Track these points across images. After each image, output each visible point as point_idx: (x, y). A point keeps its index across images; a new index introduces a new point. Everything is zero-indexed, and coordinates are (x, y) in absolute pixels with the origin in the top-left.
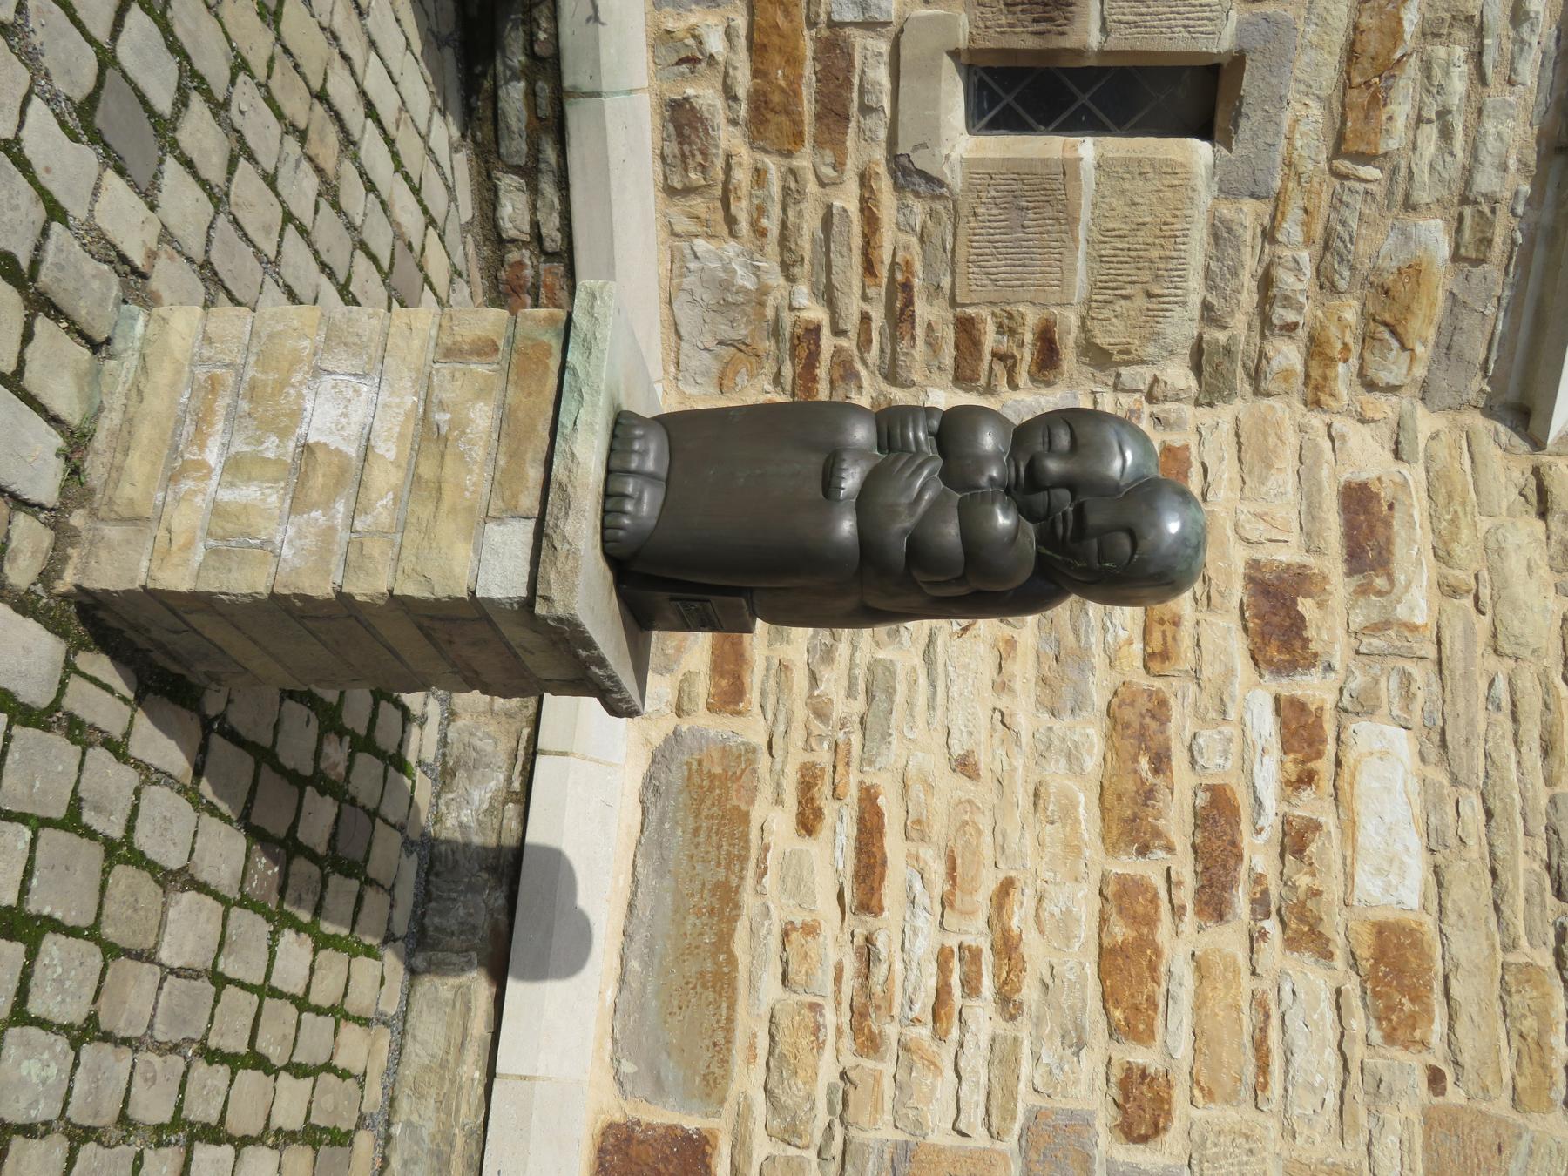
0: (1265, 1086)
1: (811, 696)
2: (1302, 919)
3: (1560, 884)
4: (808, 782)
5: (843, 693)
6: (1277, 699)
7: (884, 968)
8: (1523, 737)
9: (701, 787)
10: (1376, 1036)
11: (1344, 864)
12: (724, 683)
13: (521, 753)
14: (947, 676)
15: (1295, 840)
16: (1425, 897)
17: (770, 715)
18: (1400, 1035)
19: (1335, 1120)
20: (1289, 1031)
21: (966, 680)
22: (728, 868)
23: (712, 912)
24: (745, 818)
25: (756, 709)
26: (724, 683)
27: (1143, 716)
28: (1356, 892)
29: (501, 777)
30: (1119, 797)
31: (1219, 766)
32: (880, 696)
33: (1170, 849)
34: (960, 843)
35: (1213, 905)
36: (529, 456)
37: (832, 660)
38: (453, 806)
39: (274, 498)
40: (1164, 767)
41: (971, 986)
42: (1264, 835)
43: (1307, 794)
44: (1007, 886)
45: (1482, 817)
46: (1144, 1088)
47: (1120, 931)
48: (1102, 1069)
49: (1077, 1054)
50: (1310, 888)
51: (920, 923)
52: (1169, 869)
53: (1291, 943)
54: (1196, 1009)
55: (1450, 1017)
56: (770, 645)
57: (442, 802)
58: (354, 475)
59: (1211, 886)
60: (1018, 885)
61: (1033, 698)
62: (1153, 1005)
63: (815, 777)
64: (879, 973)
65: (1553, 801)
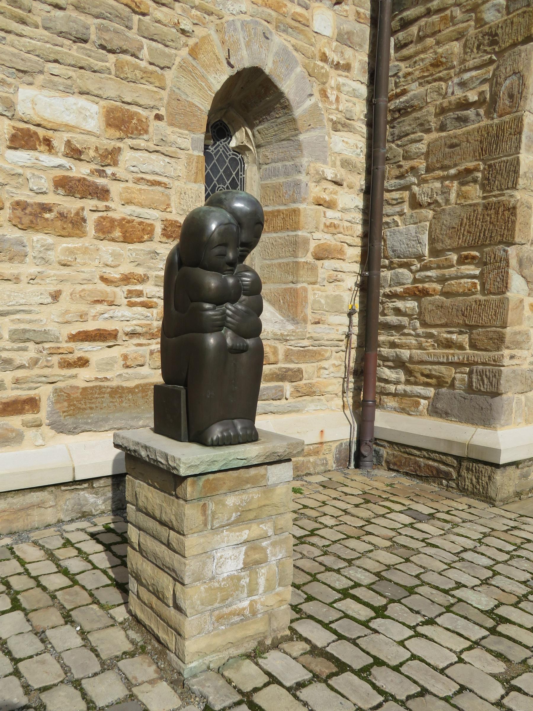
1: (28, 368)
2: (107, 157)
3: (83, 40)
4: (67, 365)
5: (26, 353)
6: (10, 148)
7: (137, 328)
8: (19, 31)
9: (74, 410)
10: (145, 137)
11: (83, 134)
12: (27, 407)
13: (72, 487)
14: (14, 305)
15: (75, 153)
16: (93, 102)
17: (39, 385)
18: (145, 127)
20: (147, 171)
21: (15, 296)
22: (104, 393)
23: (120, 397)
24: (85, 389)
25: (36, 391)
26: (27, 407)
27: (26, 214)
28: (95, 131)
29: (82, 493)
30: (64, 228)
31: (45, 183)
32: (27, 336)
33: (83, 209)
34: (88, 298)
35: (102, 193)
36: (247, 476)
37: (11, 359)
38: (97, 508)
39: (263, 571)
40: (48, 207)
41: (140, 294)
43: (55, 143)
44: (103, 279)
45: (57, 65)
46: (168, 229)
47: (117, 233)
48: (163, 245)
49: (158, 254)
51: (120, 314)
52: (91, 210)
53: (115, 164)
54: (142, 206)
55: (136, 105)
56: (5, 389)
57: (96, 513)
58: (252, 544)
60: (102, 274)
61: (19, 265)
62: (140, 223)
63: (65, 362)
64: (139, 330)
65: (46, 28)
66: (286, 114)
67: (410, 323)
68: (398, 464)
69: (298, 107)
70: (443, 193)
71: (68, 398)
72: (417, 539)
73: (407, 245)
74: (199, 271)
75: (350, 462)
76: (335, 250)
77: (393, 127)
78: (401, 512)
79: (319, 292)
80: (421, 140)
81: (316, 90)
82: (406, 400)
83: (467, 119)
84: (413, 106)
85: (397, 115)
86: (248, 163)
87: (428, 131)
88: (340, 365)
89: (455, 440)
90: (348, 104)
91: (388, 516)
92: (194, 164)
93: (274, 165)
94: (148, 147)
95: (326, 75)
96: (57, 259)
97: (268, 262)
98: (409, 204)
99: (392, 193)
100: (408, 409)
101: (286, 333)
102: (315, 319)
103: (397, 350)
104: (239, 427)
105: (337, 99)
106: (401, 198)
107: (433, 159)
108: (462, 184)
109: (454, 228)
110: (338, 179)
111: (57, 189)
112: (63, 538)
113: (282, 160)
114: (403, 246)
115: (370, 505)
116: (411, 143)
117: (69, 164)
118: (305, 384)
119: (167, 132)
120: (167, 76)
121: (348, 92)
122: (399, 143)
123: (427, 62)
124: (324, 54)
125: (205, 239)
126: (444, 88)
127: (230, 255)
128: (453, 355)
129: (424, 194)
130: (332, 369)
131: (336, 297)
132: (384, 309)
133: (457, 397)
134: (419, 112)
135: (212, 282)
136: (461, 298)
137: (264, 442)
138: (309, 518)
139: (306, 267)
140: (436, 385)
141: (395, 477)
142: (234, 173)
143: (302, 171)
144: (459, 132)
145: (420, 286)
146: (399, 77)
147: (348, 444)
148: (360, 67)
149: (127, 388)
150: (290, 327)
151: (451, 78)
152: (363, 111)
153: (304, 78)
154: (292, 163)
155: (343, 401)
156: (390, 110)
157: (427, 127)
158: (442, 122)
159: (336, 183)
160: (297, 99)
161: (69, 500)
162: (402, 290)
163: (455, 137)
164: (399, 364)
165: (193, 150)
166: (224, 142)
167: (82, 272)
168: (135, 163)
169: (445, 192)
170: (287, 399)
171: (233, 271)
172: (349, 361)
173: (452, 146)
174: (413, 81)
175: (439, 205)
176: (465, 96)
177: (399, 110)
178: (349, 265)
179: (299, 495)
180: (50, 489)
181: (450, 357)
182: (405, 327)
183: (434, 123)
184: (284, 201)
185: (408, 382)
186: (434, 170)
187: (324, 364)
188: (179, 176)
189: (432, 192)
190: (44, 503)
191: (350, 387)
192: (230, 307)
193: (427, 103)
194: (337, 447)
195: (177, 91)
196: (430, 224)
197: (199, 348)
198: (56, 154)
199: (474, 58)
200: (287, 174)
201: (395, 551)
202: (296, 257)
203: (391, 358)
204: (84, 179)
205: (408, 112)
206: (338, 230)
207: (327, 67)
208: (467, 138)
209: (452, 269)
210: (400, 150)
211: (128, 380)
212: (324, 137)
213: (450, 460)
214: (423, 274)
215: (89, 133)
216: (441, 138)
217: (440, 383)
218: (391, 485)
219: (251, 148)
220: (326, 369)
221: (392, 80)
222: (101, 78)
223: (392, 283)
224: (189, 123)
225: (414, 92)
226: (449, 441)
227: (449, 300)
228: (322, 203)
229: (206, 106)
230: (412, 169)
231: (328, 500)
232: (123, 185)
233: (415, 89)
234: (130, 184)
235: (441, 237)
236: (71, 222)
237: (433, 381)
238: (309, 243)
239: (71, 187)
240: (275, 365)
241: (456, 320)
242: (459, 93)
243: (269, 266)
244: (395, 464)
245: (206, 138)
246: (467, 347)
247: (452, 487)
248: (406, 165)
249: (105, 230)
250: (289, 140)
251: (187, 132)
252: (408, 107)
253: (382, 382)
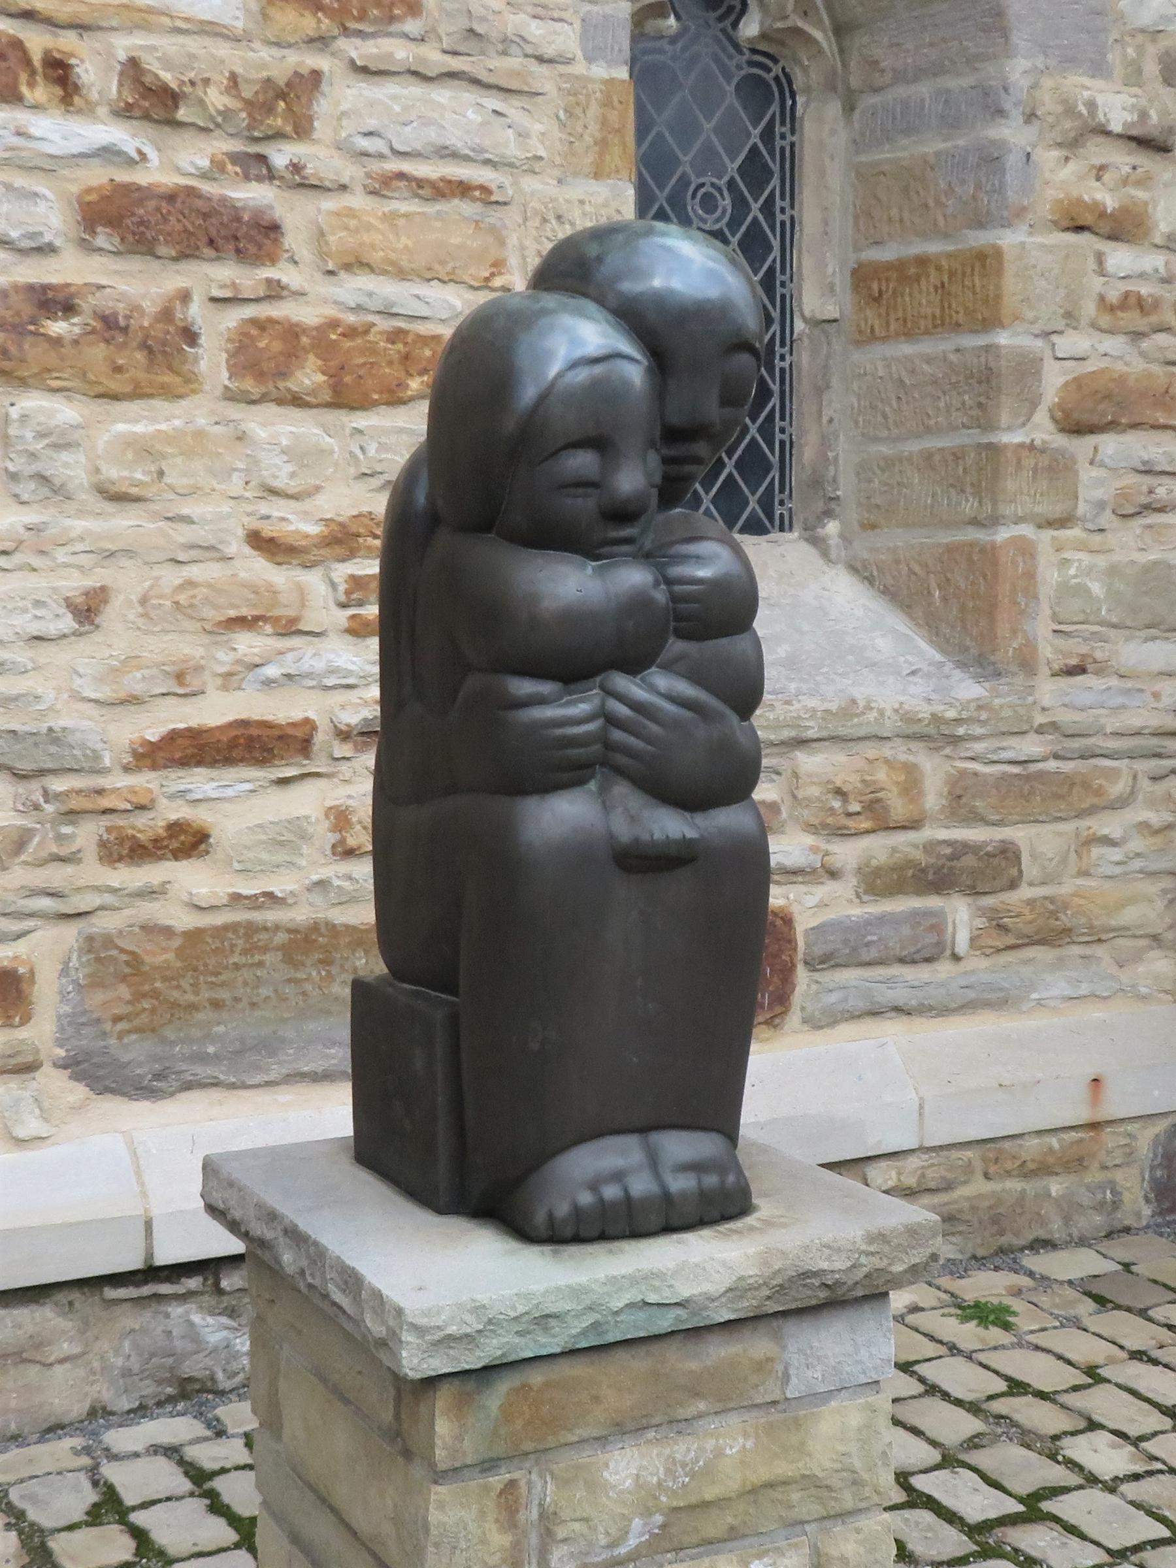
0: (484, 189)
2: (270, 109)
9: (153, 1011)
10: (412, 26)
13: (146, 1290)
15: (154, 102)
19: (516, 102)
20: (418, 146)
22: (265, 949)
23: (326, 962)
24: (194, 936)
28: (226, 20)
29: (177, 1310)
30: (118, 369)
33: (185, 297)
35: (255, 238)
36: (694, 1365)
38: (235, 1366)
40: (60, 296)
42: (148, 150)
43: (87, 72)
44: (261, 542)
47: (309, 376)
50: (228, 91)
53: (302, 130)
54: (402, 274)
59: (236, 238)
60: (256, 525)
62: (396, 336)
63: (121, 841)
86: (808, 90)
92: (594, 110)
93: (902, 91)
94: (423, 60)
97: (884, 449)
101: (951, 714)
102: (1066, 655)
111: (93, 233)
112: (95, 1484)
113: (937, 70)
118: (1031, 902)
130: (1137, 844)
135: (567, 585)
137: (769, 1224)
138: (1026, 1438)
139: (1029, 462)
142: (756, 132)
143: (1007, 106)
150: (969, 689)
154: (966, 81)
161: (127, 1338)
165: (590, 59)
168: (372, 123)
170: (956, 958)
179: (996, 1334)
180: (62, 1297)
184: (941, 222)
187: (1109, 825)
190: (39, 1346)
194: (1156, 1141)
197: (502, 859)
198: (88, 111)
200: (951, 123)
204: (191, 192)
206: (1154, 319)
215: (208, 29)
219: (818, 35)
228: (1088, 219)
231: (1111, 1361)
238: (1037, 374)
240: (911, 836)
243: (888, 464)
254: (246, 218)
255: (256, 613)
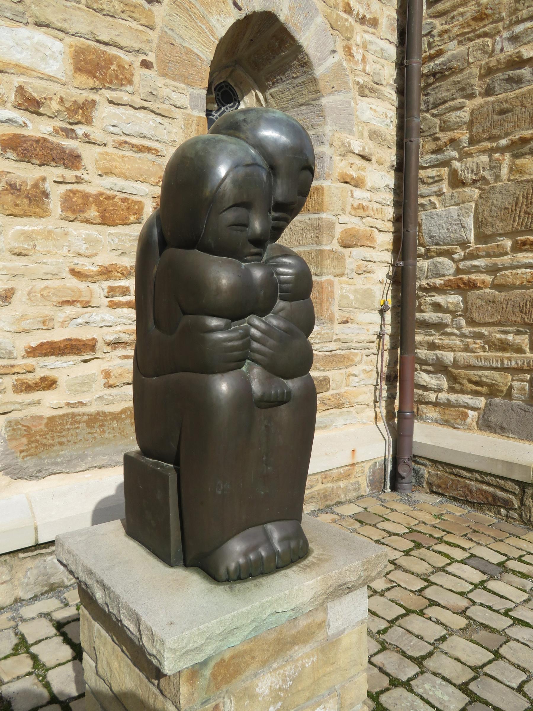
2: (75, 112)
9: (36, 447)
10: (129, 88)
11: (42, 79)
13: (35, 553)
16: (56, 37)
18: (128, 76)
20: (132, 132)
22: (79, 422)
24: (51, 419)
28: (59, 76)
30: (17, 205)
33: (44, 179)
34: (54, 298)
35: (72, 160)
44: (74, 272)
47: (93, 213)
51: (98, 318)
52: (55, 182)
53: (89, 121)
54: (127, 178)
55: (116, 46)
57: (69, 584)
60: (73, 266)
62: (124, 200)
63: (22, 384)
66: (305, 72)
67: (452, 321)
68: (443, 486)
69: (320, 65)
70: (491, 168)
71: (28, 432)
72: (498, 612)
73: (448, 229)
74: (197, 256)
75: (385, 483)
76: (364, 236)
77: (427, 94)
78: (463, 562)
79: (347, 286)
80: (463, 107)
81: (339, 45)
82: (450, 411)
83: (521, 79)
84: (451, 69)
85: (432, 80)
87: (471, 96)
88: (372, 370)
89: (516, 461)
90: (375, 66)
91: (449, 569)
92: (194, 126)
94: (133, 101)
95: (350, 29)
96: (8, 247)
98: (449, 182)
99: (427, 170)
100: (452, 422)
102: (343, 317)
103: (438, 352)
104: (276, 536)
105: (364, 58)
106: (439, 176)
107: (477, 129)
108: (516, 156)
109: (506, 208)
110: (366, 153)
114: (442, 231)
115: (423, 551)
116: (449, 112)
117: (23, 119)
118: (333, 395)
119: (157, 83)
120: (156, 13)
121: (375, 51)
122: (435, 112)
123: (468, 16)
124: (348, 4)
125: (208, 192)
126: (490, 44)
127: (257, 225)
128: (509, 359)
129: (468, 169)
130: (362, 376)
131: (365, 291)
132: (420, 304)
133: (514, 408)
134: (459, 75)
135: (223, 275)
136: (518, 292)
140: (487, 394)
141: (440, 503)
143: (325, 141)
144: (510, 95)
145: (465, 277)
146: (433, 36)
147: (383, 463)
148: (388, 23)
149: (111, 414)
151: (499, 32)
152: (392, 76)
153: (325, 30)
155: (376, 412)
156: (423, 75)
157: (469, 91)
158: (488, 85)
159: (363, 157)
160: (319, 55)
162: (442, 282)
163: (506, 101)
164: (440, 368)
165: (193, 109)
166: (230, 107)
167: (45, 263)
168: (115, 122)
169: (495, 166)
171: (260, 255)
172: (382, 366)
173: (502, 112)
174: (451, 39)
175: (487, 182)
176: (519, 52)
177: (434, 74)
178: (379, 253)
181: (505, 362)
182: (446, 325)
183: (478, 86)
185: (451, 390)
186: (479, 141)
187: (354, 370)
188: (175, 141)
189: (477, 167)
191: (383, 396)
192: (257, 322)
193: (469, 64)
195: (170, 32)
196: (476, 205)
197: (200, 404)
199: (528, 7)
201: (475, 637)
202: (320, 244)
203: (431, 362)
204: (45, 140)
205: (445, 76)
206: (367, 213)
207: (351, 20)
208: (522, 102)
209: (506, 257)
210: (437, 121)
211: (111, 403)
212: (350, 103)
213: (509, 485)
214: (469, 263)
215: (50, 78)
216: (487, 103)
217: (492, 391)
218: (439, 516)
220: (356, 376)
221: (425, 40)
222: (66, 6)
223: (430, 274)
224: (186, 74)
225: (452, 52)
226: (509, 463)
227: (503, 294)
228: (348, 180)
229: (208, 55)
230: (452, 141)
232: (101, 149)
233: (453, 49)
234: (110, 149)
235: (490, 219)
236: (27, 197)
237: (484, 389)
238: (334, 227)
239: (26, 150)
241: (512, 318)
242: (510, 49)
244: (439, 486)
245: (208, 102)
246: (528, 350)
247: (513, 519)
248: (445, 137)
249: (75, 208)
250: (309, 104)
251: (183, 86)
252: (446, 70)
253: (419, 389)
254: (67, 152)
255: (74, 299)
